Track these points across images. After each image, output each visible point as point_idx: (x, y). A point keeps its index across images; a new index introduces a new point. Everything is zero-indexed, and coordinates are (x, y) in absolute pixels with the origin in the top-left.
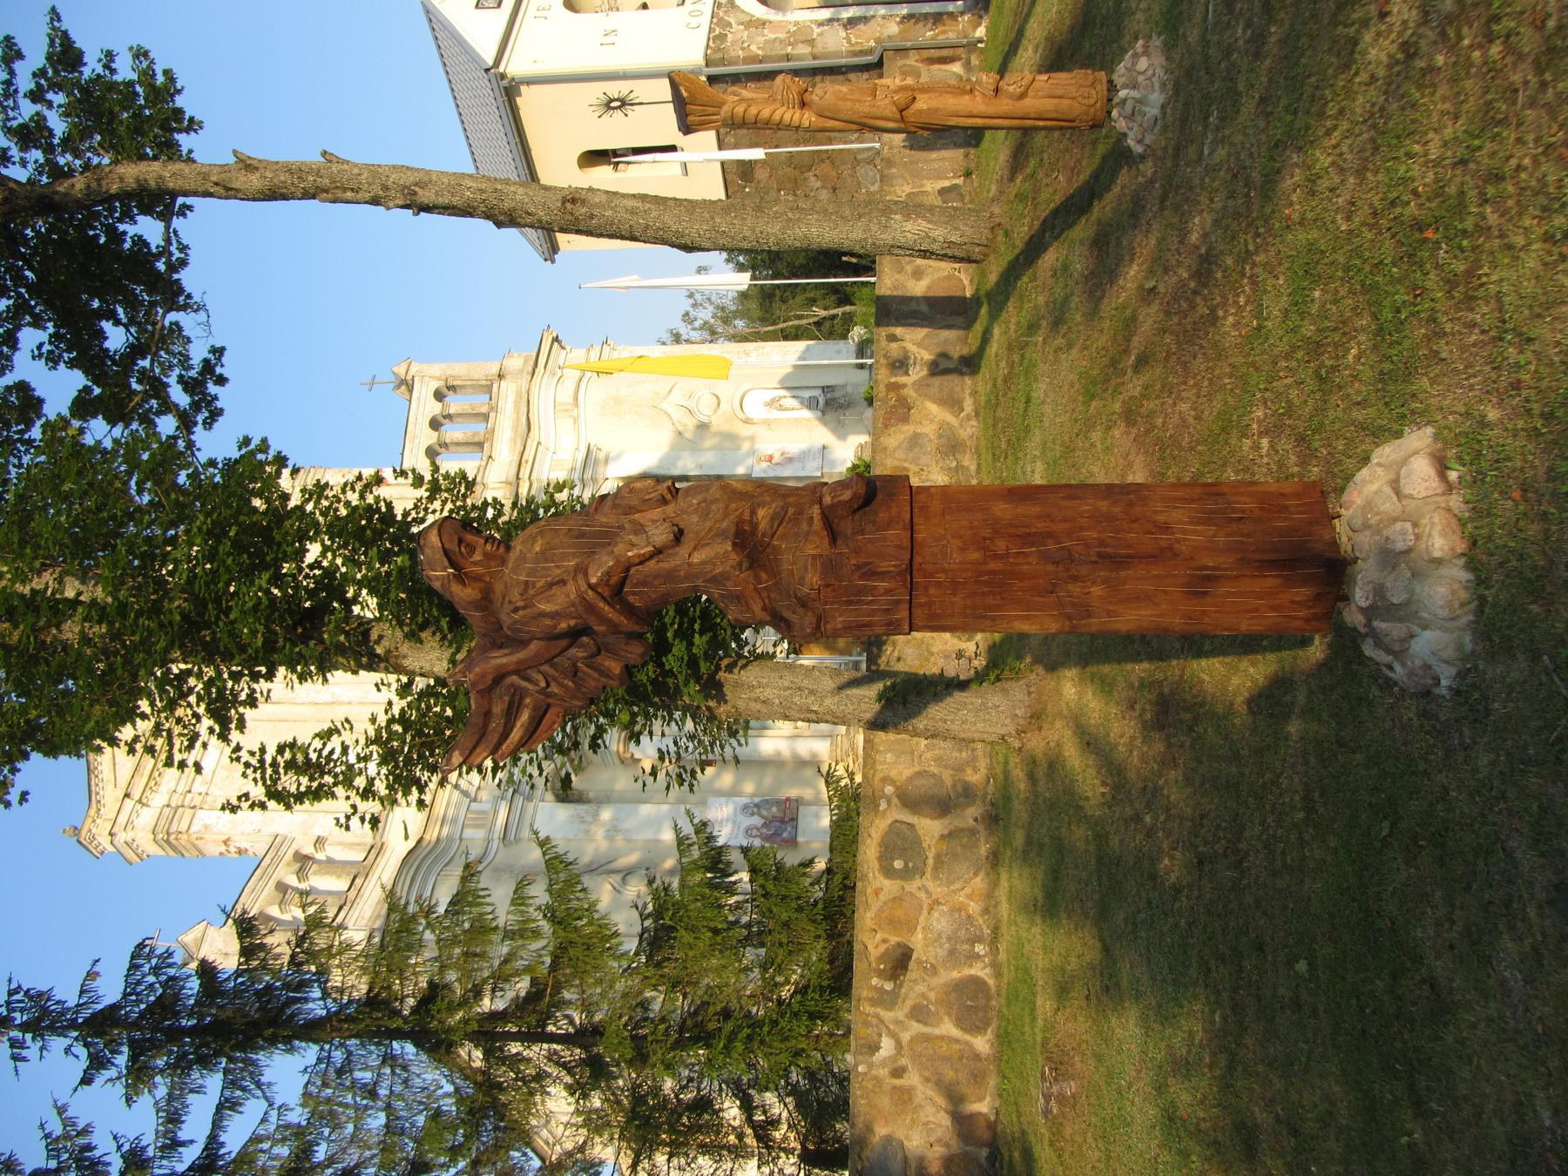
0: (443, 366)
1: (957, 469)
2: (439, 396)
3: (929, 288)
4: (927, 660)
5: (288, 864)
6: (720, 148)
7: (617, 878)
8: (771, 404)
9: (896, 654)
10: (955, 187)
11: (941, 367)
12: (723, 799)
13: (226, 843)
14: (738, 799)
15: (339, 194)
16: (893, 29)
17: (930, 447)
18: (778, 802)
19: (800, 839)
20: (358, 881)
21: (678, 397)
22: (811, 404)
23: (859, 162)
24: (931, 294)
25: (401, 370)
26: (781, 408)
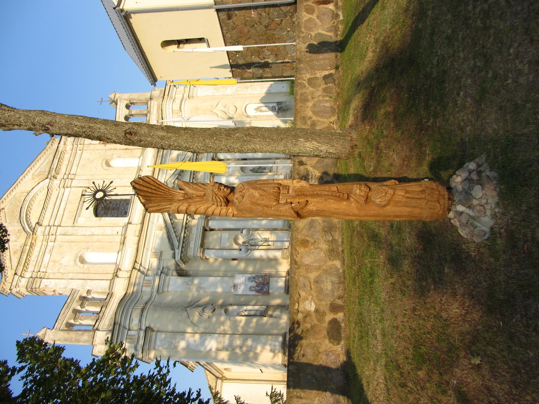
0: (129, 94)
1: (332, 241)
2: (128, 107)
4: (317, 356)
5: (77, 302)
6: (226, 45)
7: (200, 309)
8: (257, 109)
9: (302, 352)
10: (331, 75)
11: (325, 180)
12: (241, 275)
13: (54, 291)
14: (246, 275)
15: (11, 127)
17: (319, 228)
18: (262, 276)
19: (270, 291)
21: (220, 107)
22: (273, 109)
25: (112, 96)
26: (261, 111)
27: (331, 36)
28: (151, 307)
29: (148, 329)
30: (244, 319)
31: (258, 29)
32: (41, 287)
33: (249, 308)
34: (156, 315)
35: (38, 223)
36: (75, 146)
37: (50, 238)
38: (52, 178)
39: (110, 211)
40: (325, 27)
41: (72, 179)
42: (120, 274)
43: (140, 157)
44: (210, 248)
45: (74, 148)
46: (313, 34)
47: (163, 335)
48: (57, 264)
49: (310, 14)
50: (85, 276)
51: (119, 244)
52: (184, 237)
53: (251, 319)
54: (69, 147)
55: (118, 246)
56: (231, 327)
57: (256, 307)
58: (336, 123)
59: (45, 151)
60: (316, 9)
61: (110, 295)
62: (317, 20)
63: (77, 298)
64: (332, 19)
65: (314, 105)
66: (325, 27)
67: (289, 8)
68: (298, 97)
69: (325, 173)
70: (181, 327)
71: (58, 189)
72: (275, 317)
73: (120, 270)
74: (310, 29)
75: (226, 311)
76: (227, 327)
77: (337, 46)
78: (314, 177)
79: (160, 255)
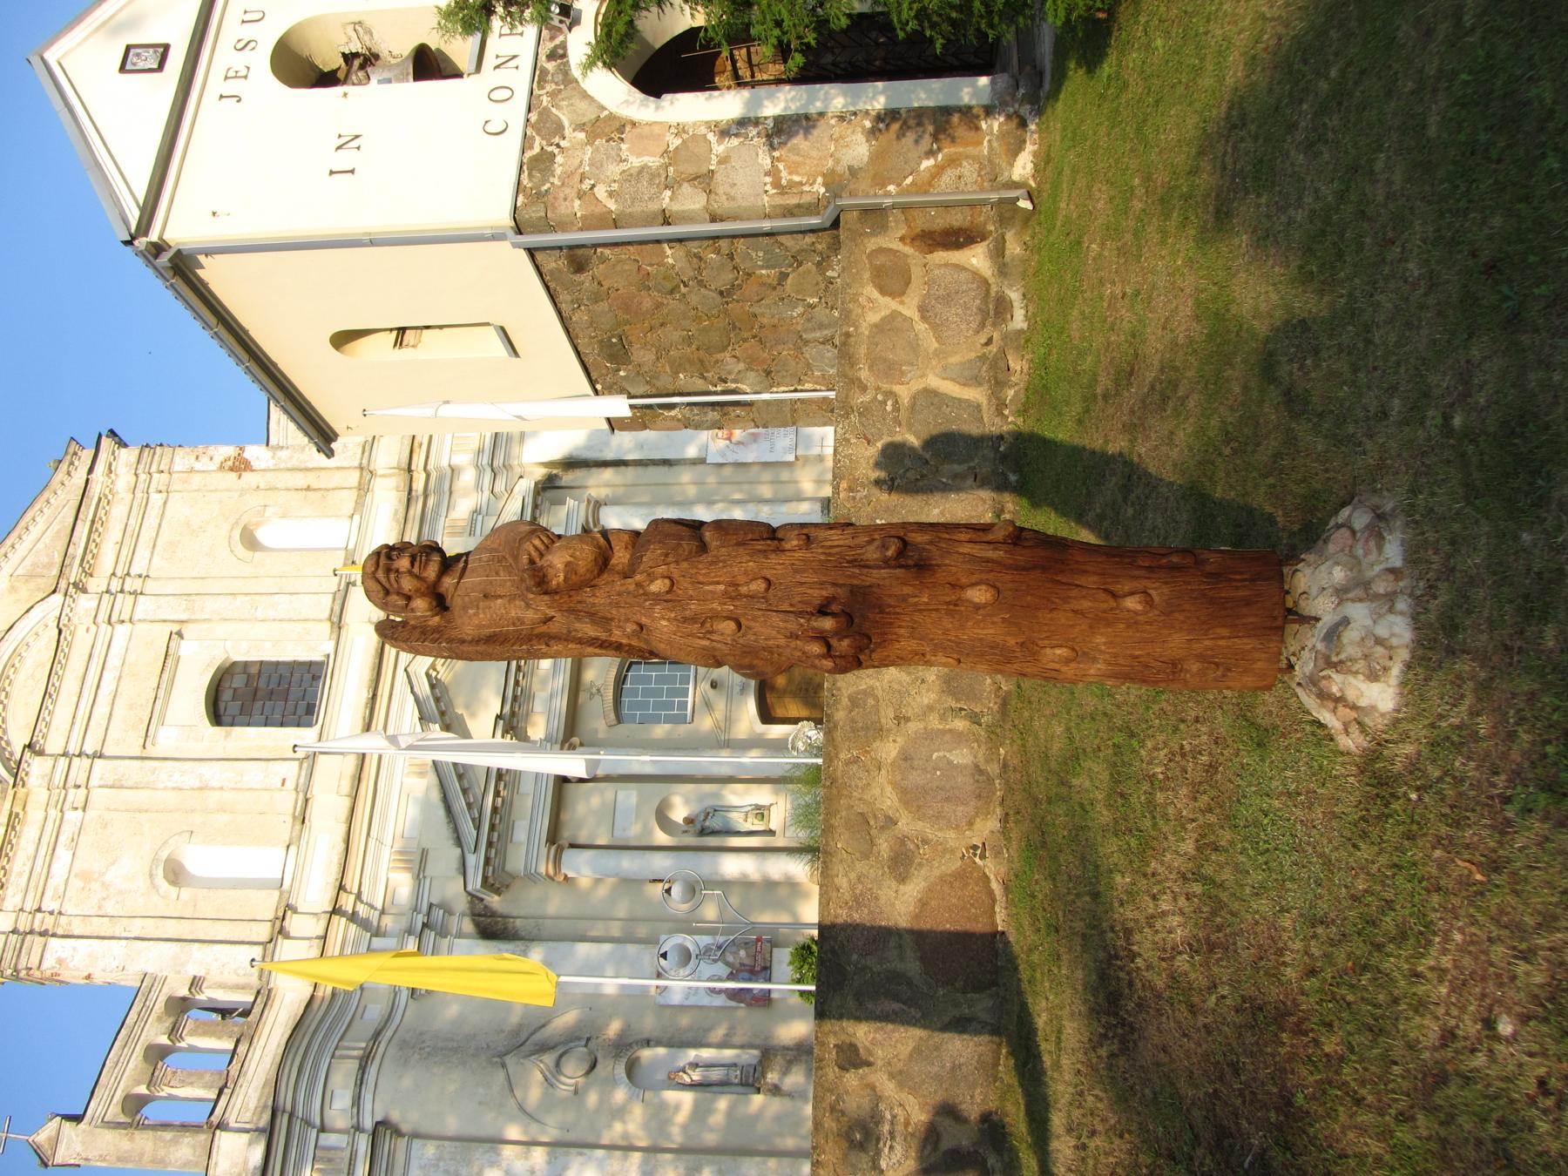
3: (923, 904)
5: (159, 1019)
7: (549, 1058)
11: (946, 1144)
13: (88, 977)
16: (858, 149)
20: (242, 1049)
23: (806, 343)
24: (927, 924)
27: (978, 407)
28: (392, 1051)
29: (383, 1127)
30: (687, 1098)
31: (694, 299)
32: (45, 965)
33: (707, 1054)
34: (407, 1082)
35: (29, 746)
36: (143, 477)
37: (70, 798)
38: (72, 590)
39: (258, 704)
40: (953, 360)
41: (134, 593)
42: (294, 924)
43: (352, 517)
44: (582, 840)
45: (141, 486)
46: (904, 393)
47: (430, 1150)
48: (95, 886)
49: (893, 295)
50: (183, 930)
51: (290, 820)
52: (495, 810)
53: (713, 1101)
54: (124, 479)
55: (285, 828)
56: (646, 1126)
57: (728, 1054)
58: (997, 854)
59: (46, 494)
60: (917, 272)
61: (264, 994)
62: (921, 327)
63: (160, 1006)
64: (982, 325)
65: (905, 757)
66: (953, 360)
67: (809, 239)
68: (840, 715)
69: (948, 1111)
70: (487, 1123)
71: (93, 628)
72: (790, 1095)
73: (295, 911)
74: (891, 370)
75: (632, 1069)
76: (633, 1125)
77: (1004, 458)
78: (899, 1128)
79: (419, 862)
